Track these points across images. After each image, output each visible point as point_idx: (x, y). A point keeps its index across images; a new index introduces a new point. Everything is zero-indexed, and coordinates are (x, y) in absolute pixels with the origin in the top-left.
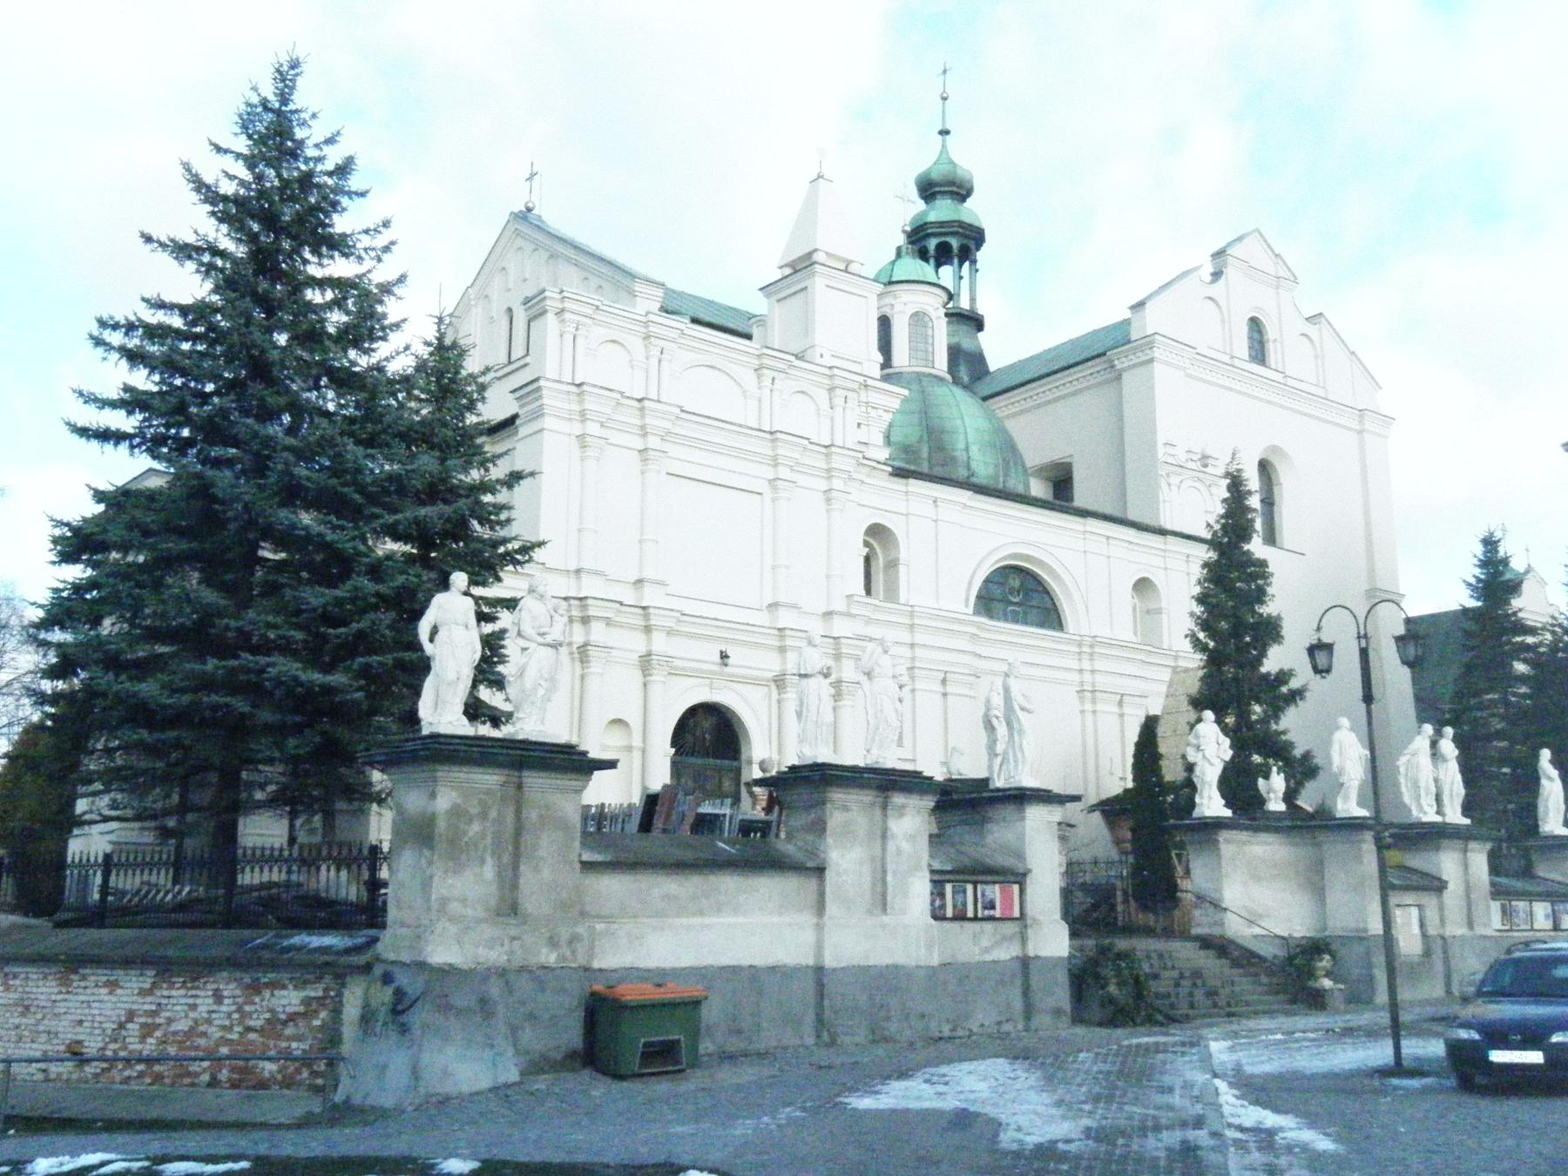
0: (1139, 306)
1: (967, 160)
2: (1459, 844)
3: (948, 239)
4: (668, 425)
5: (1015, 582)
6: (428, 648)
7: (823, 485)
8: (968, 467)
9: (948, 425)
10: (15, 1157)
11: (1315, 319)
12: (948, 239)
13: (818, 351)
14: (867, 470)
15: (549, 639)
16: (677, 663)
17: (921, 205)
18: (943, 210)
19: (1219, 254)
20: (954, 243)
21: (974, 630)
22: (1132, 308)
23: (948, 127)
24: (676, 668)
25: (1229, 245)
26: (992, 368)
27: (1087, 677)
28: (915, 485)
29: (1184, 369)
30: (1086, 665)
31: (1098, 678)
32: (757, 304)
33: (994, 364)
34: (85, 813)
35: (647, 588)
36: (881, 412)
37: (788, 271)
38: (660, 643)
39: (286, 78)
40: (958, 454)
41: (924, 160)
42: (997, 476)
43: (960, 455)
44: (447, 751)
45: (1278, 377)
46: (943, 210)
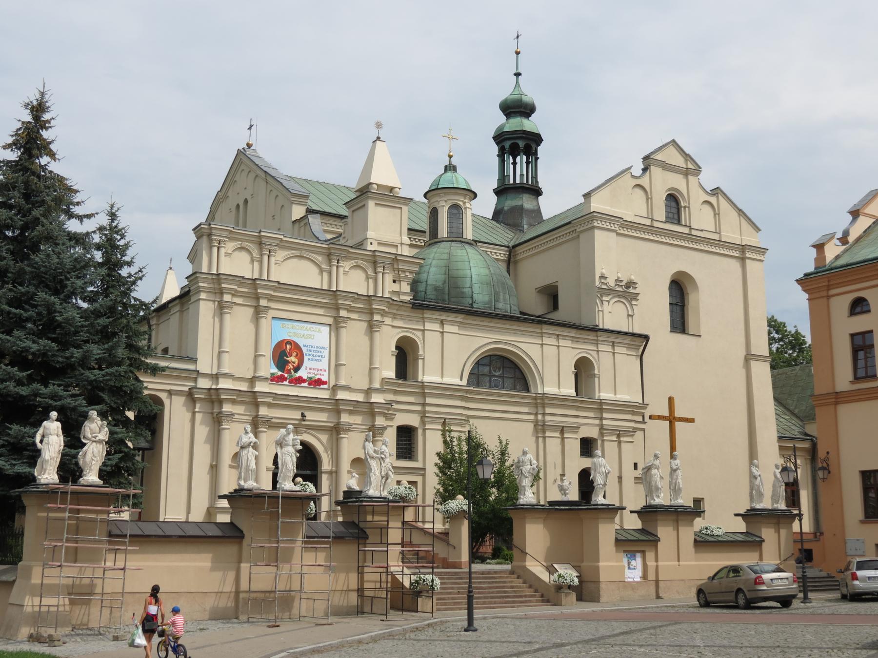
0: (587, 196)
3: (517, 141)
6: (39, 445)
7: (366, 317)
9: (461, 273)
10: (470, 633)
11: (716, 192)
12: (517, 141)
13: (369, 241)
14: (397, 307)
16: (273, 420)
17: (502, 118)
18: (517, 123)
19: (646, 158)
20: (521, 144)
22: (584, 196)
23: (519, 71)
25: (653, 153)
26: (545, 218)
27: (540, 417)
28: (428, 314)
30: (540, 411)
31: (547, 418)
32: (344, 211)
33: (546, 215)
34: (837, 257)
35: (374, 395)
36: (407, 274)
37: (358, 194)
38: (263, 411)
40: (465, 290)
41: (505, 92)
42: (490, 301)
43: (467, 291)
44: (49, 493)
45: (686, 230)
46: (517, 123)
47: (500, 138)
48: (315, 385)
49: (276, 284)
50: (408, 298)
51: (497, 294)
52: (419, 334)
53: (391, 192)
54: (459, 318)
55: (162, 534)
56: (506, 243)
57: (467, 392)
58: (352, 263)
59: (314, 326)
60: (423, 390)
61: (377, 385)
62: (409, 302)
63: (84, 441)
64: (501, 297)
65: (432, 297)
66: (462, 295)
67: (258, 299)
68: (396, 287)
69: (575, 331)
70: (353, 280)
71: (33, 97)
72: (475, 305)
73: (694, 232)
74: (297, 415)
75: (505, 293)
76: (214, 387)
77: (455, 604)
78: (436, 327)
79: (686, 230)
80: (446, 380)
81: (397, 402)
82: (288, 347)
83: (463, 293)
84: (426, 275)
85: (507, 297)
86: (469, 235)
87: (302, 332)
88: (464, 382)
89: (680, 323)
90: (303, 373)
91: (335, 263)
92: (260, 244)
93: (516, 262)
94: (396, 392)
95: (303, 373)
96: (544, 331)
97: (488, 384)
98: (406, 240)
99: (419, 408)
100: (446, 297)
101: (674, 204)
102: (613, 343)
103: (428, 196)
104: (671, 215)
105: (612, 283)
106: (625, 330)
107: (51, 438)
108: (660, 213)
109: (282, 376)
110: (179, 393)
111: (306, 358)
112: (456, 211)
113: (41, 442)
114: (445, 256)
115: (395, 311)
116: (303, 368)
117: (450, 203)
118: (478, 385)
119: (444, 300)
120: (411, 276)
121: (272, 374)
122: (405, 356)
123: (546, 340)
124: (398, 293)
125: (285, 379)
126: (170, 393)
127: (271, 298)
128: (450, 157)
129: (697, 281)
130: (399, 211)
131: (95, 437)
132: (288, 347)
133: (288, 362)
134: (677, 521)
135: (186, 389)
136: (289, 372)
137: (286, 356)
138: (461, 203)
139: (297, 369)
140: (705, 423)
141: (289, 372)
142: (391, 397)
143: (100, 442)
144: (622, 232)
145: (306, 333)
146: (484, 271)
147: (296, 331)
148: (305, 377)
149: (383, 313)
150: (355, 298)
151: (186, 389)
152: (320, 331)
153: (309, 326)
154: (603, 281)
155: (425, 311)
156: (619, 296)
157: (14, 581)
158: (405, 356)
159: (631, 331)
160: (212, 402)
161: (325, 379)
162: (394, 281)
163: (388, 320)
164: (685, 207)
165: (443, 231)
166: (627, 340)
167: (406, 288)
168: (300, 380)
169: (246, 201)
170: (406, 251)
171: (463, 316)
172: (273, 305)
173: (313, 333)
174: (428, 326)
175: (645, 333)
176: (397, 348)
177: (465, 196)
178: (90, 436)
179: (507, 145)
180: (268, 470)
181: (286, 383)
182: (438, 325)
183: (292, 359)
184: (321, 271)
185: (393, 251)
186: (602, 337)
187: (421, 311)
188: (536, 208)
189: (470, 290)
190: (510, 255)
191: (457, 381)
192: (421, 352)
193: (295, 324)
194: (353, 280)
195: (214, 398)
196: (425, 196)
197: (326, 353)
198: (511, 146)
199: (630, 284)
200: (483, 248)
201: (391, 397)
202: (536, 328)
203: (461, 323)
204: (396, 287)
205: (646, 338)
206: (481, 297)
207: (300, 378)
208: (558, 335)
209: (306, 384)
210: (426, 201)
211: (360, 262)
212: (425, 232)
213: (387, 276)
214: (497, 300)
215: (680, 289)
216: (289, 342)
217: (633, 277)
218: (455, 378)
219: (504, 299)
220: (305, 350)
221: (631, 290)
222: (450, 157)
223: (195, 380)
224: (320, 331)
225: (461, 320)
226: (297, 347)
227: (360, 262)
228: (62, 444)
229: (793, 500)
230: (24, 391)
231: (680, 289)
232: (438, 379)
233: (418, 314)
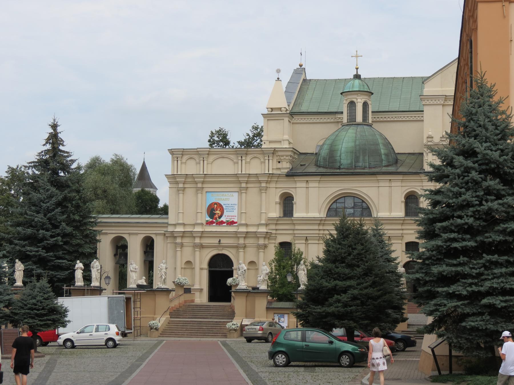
36: (285, 157)
42: (352, 163)
43: (338, 158)
48: (230, 225)
59: (230, 193)
65: (322, 163)
66: (335, 161)
69: (402, 176)
71: (51, 122)
74: (216, 241)
77: (175, 335)
78: (304, 185)
82: (215, 206)
83: (336, 160)
85: (367, 158)
87: (223, 198)
90: (223, 219)
91: (267, 158)
95: (223, 219)
96: (378, 178)
109: (212, 221)
111: (225, 211)
116: (224, 216)
117: (348, 101)
121: (207, 221)
122: (287, 202)
123: (381, 184)
125: (214, 223)
126: (156, 234)
128: (357, 69)
132: (215, 206)
133: (215, 214)
136: (216, 219)
137: (214, 211)
139: (220, 217)
141: (216, 219)
143: (20, 270)
144: (446, 103)
145: (225, 197)
147: (219, 197)
148: (225, 221)
151: (163, 232)
152: (232, 196)
153: (226, 194)
154: (429, 140)
158: (287, 202)
161: (235, 220)
168: (222, 222)
173: (229, 197)
174: (298, 185)
181: (214, 224)
183: (218, 212)
193: (219, 193)
195: (173, 236)
197: (236, 207)
202: (373, 178)
203: (320, 181)
206: (345, 160)
207: (222, 221)
208: (390, 180)
209: (225, 224)
211: (255, 155)
216: (216, 203)
219: (364, 160)
220: (224, 207)
222: (357, 69)
224: (232, 196)
225: (402, 178)
226: (220, 206)
227: (255, 155)
233: (291, 179)
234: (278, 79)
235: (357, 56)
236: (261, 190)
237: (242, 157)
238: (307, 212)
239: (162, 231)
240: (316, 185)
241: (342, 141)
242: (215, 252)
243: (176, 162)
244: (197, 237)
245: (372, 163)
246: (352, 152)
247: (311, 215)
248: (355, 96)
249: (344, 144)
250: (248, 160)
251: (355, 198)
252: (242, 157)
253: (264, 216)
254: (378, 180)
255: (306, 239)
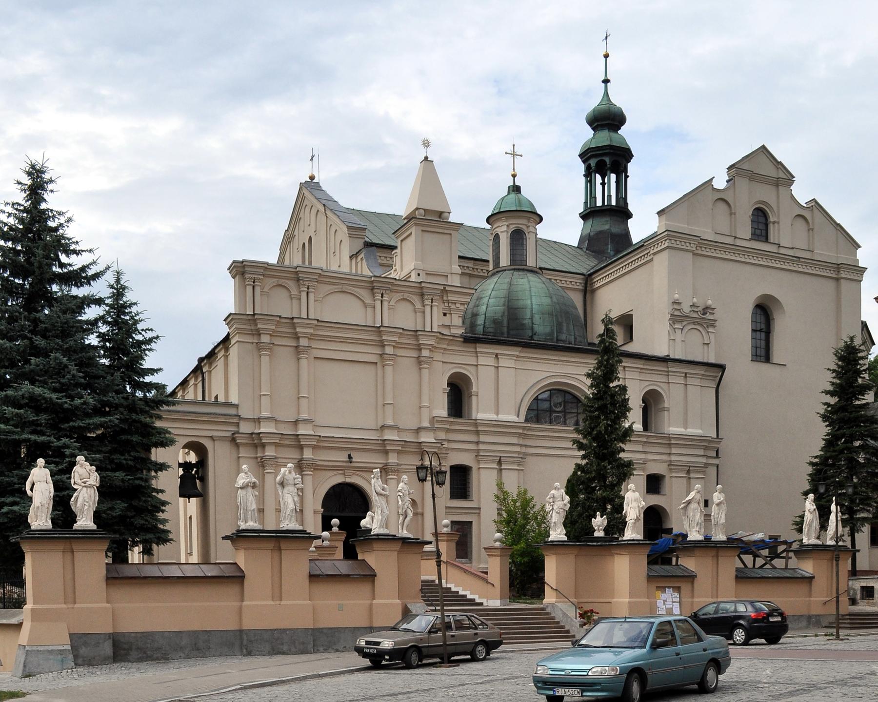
1: (619, 100)
2: (714, 552)
3: (604, 158)
4: (311, 331)
5: (558, 399)
6: (29, 492)
7: (415, 354)
8: (532, 329)
9: (521, 303)
12: (604, 158)
15: (87, 484)
17: (589, 133)
21: (521, 431)
24: (318, 466)
28: (481, 348)
29: (692, 251)
35: (300, 426)
36: (458, 305)
38: (308, 454)
39: (37, 184)
40: (526, 322)
41: (593, 102)
42: (552, 333)
43: (527, 322)
45: (773, 249)
47: (586, 155)
49: (316, 322)
50: (460, 331)
51: (560, 325)
52: (472, 369)
53: (440, 217)
54: (515, 351)
55: (160, 575)
56: (584, 271)
57: (524, 428)
58: (398, 296)
60: (477, 428)
61: (426, 424)
62: (461, 336)
63: (75, 487)
64: (565, 328)
65: (491, 330)
66: (522, 326)
67: (297, 338)
68: (446, 320)
69: (643, 362)
70: (402, 316)
72: (535, 338)
73: (782, 251)
75: (568, 324)
76: (256, 431)
78: (491, 361)
79: (773, 249)
80: (502, 417)
81: (449, 441)
83: (523, 325)
84: (485, 307)
85: (571, 327)
86: (531, 262)
88: (522, 418)
89: (763, 352)
91: (427, 302)
92: (298, 280)
93: (594, 291)
94: (448, 431)
97: (548, 419)
98: (456, 269)
99: (472, 447)
100: (505, 330)
101: (762, 220)
102: (686, 374)
103: (491, 220)
104: (758, 232)
105: (686, 309)
106: (699, 359)
107: (40, 481)
108: (745, 230)
110: (221, 439)
112: (518, 237)
113: (32, 490)
114: (506, 286)
115: (445, 346)
118: (538, 421)
119: (503, 333)
120: (462, 308)
122: (458, 395)
124: (449, 327)
126: (212, 438)
127: (311, 337)
128: (514, 176)
129: (784, 305)
130: (448, 236)
131: (85, 483)
134: (717, 557)
135: (229, 434)
138: (524, 227)
140: (746, 453)
142: (442, 435)
143: (91, 486)
144: (700, 252)
146: (547, 301)
149: (432, 349)
150: (401, 334)
155: (478, 345)
156: (694, 323)
157: (22, 623)
158: (458, 395)
159: (705, 361)
160: (255, 446)
162: (445, 314)
163: (438, 356)
164: (774, 223)
165: (504, 261)
166: (701, 371)
167: (457, 321)
169: (310, 238)
170: (456, 281)
171: (520, 349)
172: (314, 344)
175: (722, 362)
176: (449, 384)
177: (529, 219)
178: (79, 481)
179: (593, 162)
180: (315, 512)
182: (492, 359)
184: (365, 305)
185: (442, 281)
186: (673, 367)
187: (473, 345)
188: (624, 232)
189: (530, 321)
190: (586, 284)
191: (514, 418)
192: (474, 389)
194: (402, 316)
195: (257, 442)
196: (488, 220)
198: (597, 164)
199: (707, 309)
200: (548, 275)
201: (442, 435)
203: (517, 356)
204: (446, 320)
205: (722, 368)
206: (542, 327)
210: (488, 227)
211: (406, 295)
212: (488, 261)
213: (435, 309)
214: (560, 331)
215: (764, 313)
217: (710, 302)
218: (511, 414)
219: (568, 330)
221: (708, 316)
222: (514, 176)
223: (238, 425)
225: (517, 353)
227: (406, 295)
228: (52, 490)
229: (318, 576)
230: (65, 440)
231: (764, 313)
232: (493, 417)
233: (470, 348)
234: (426, 158)
235: (514, 154)
236: (419, 361)
237: (382, 295)
238: (686, 428)
239: (225, 431)
240: (510, 363)
241: (527, 293)
242: (339, 479)
243: (249, 289)
244: (308, 446)
245: (578, 339)
246: (550, 314)
247: (691, 431)
248: (524, 221)
249: (533, 298)
250: (392, 303)
251: (567, 395)
252: (382, 295)
253: (425, 412)
254: (668, 372)
255: (500, 463)
